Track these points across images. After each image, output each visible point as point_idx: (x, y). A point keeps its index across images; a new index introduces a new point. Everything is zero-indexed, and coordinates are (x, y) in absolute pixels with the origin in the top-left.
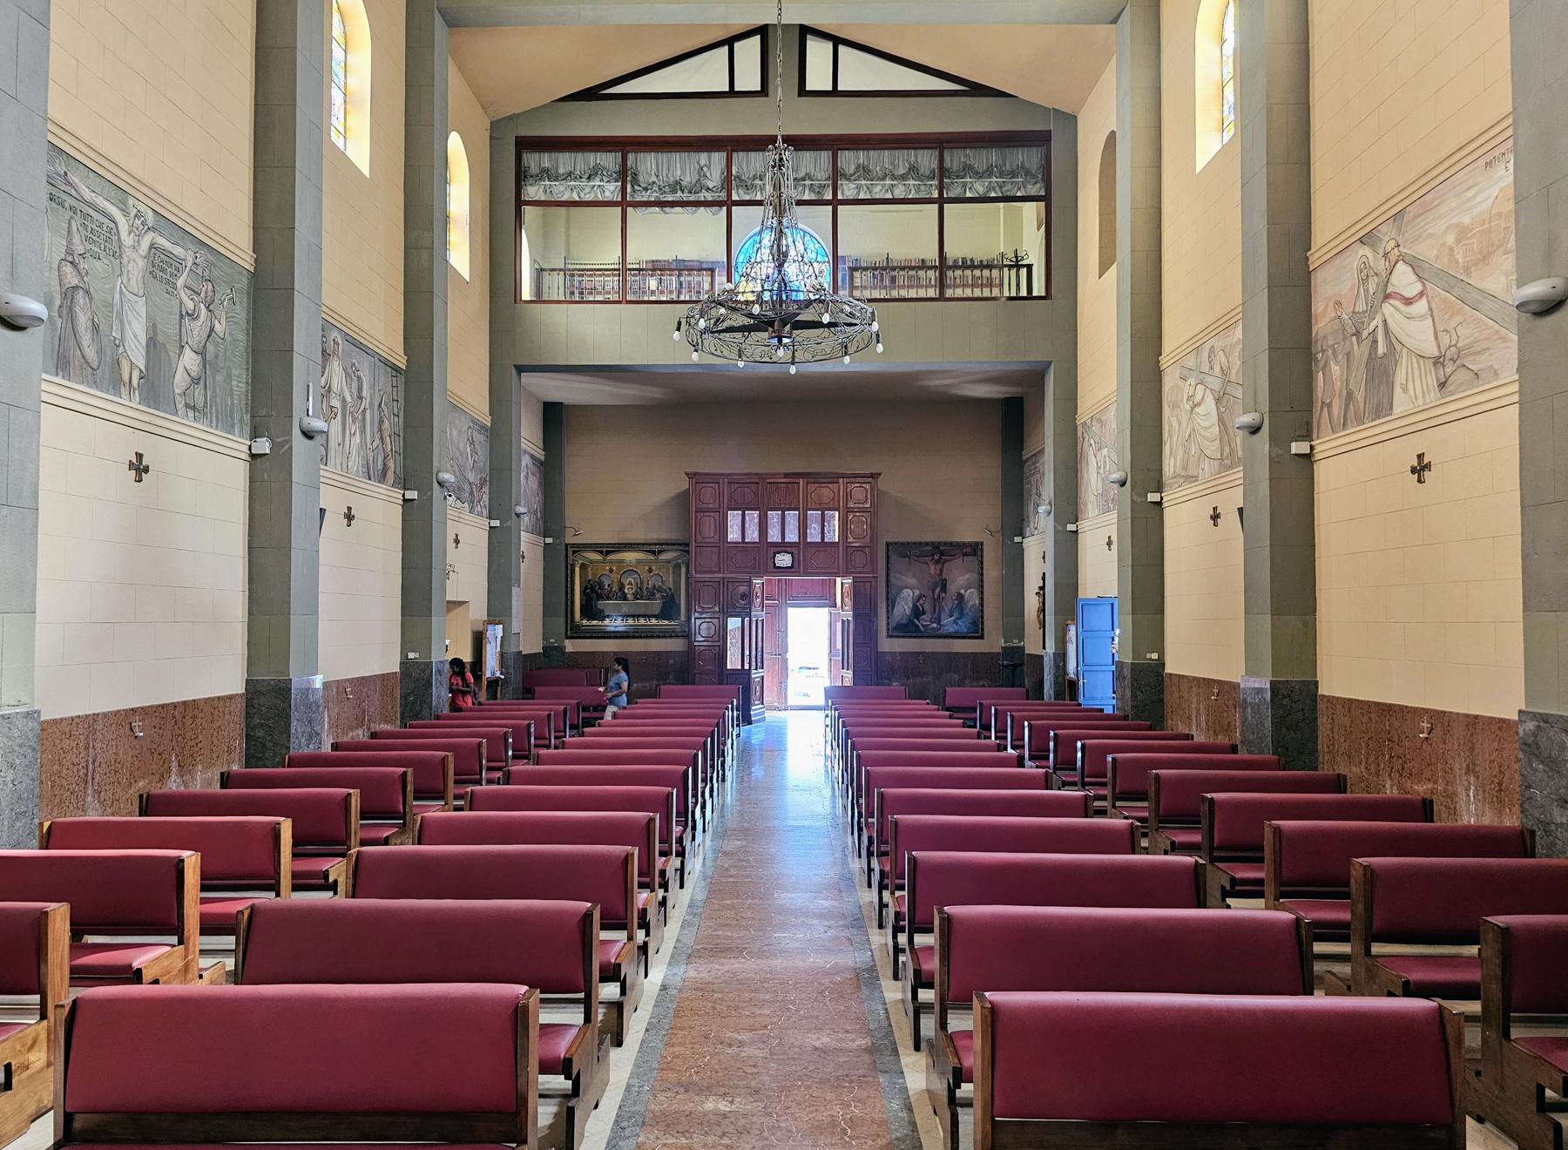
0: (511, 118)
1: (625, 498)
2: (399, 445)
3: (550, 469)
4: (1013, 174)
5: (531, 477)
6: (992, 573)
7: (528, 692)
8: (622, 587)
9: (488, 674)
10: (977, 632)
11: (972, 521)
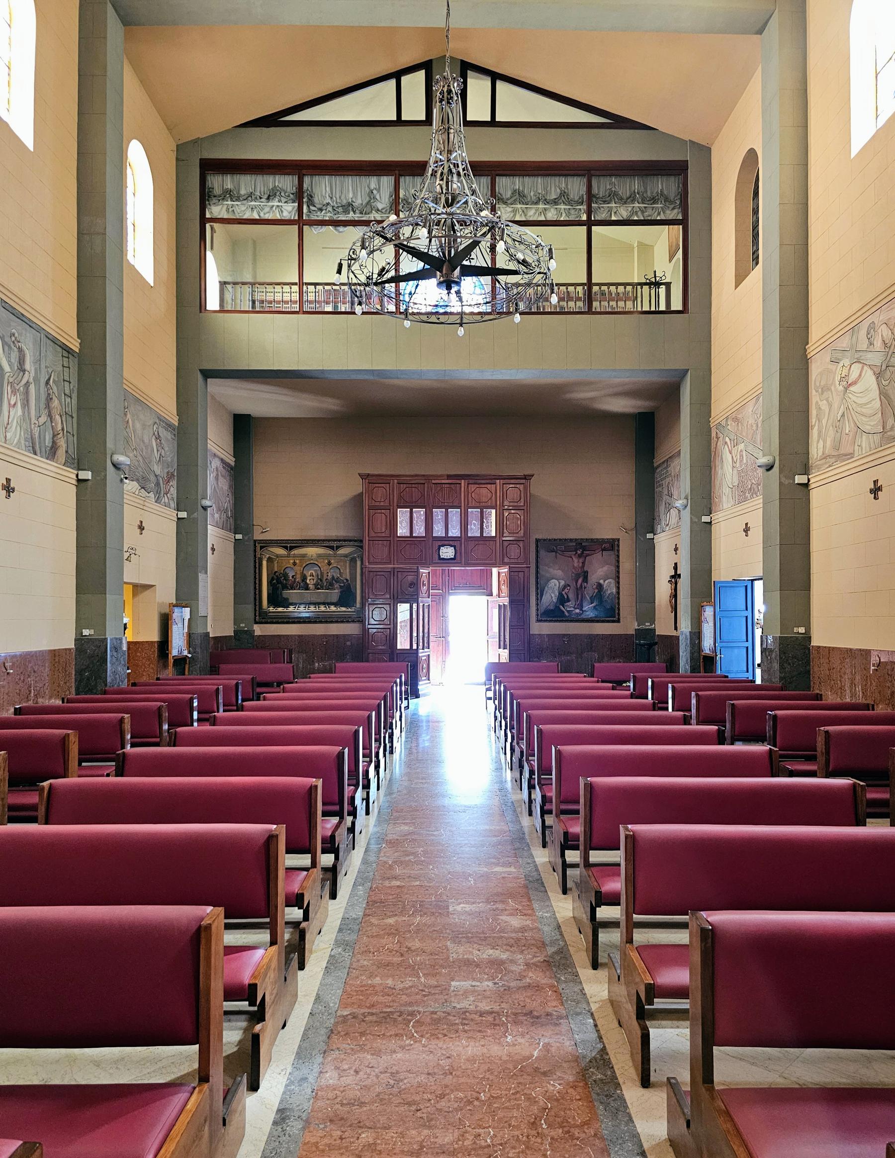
0: (195, 142)
1: (308, 499)
2: (72, 426)
3: (240, 474)
4: (654, 200)
5: (221, 479)
6: (627, 565)
7: (214, 670)
8: (304, 578)
9: (174, 652)
10: (612, 614)
11: (609, 519)
